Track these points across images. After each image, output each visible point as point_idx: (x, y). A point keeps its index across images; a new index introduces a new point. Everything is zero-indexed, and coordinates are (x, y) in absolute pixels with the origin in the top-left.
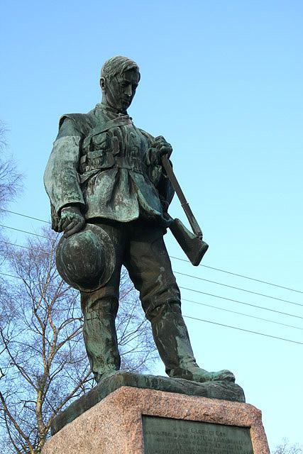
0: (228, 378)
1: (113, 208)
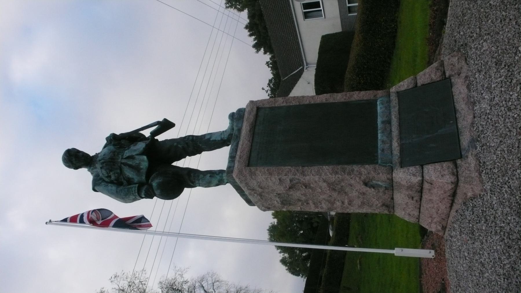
0: (232, 116)
1: (142, 169)
